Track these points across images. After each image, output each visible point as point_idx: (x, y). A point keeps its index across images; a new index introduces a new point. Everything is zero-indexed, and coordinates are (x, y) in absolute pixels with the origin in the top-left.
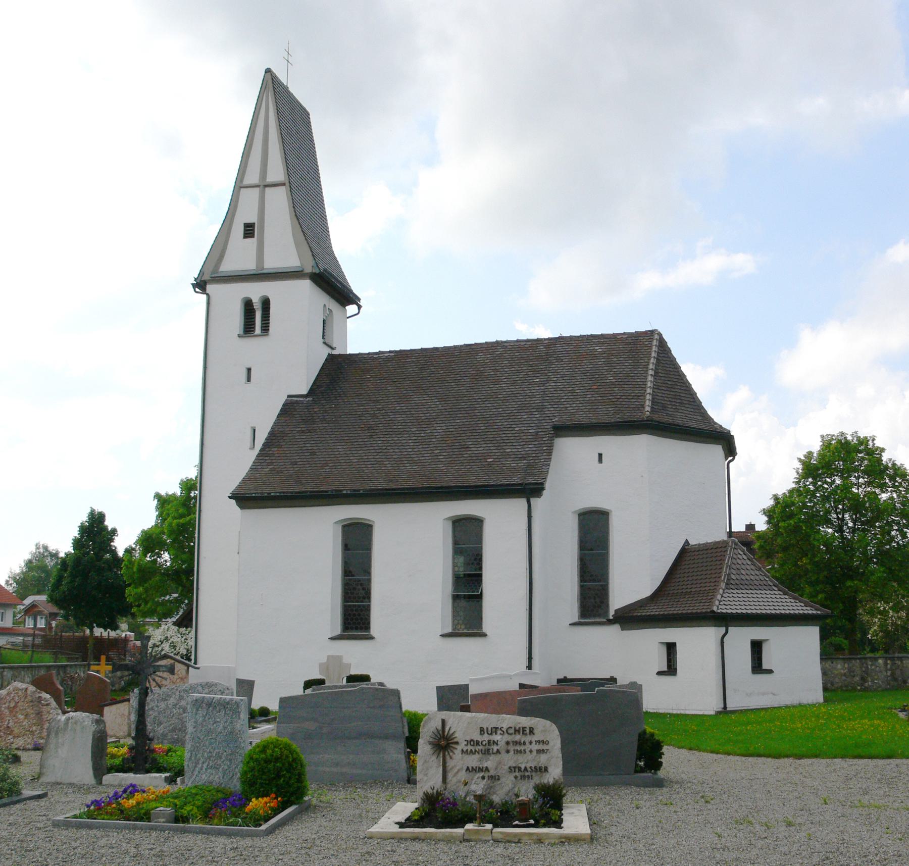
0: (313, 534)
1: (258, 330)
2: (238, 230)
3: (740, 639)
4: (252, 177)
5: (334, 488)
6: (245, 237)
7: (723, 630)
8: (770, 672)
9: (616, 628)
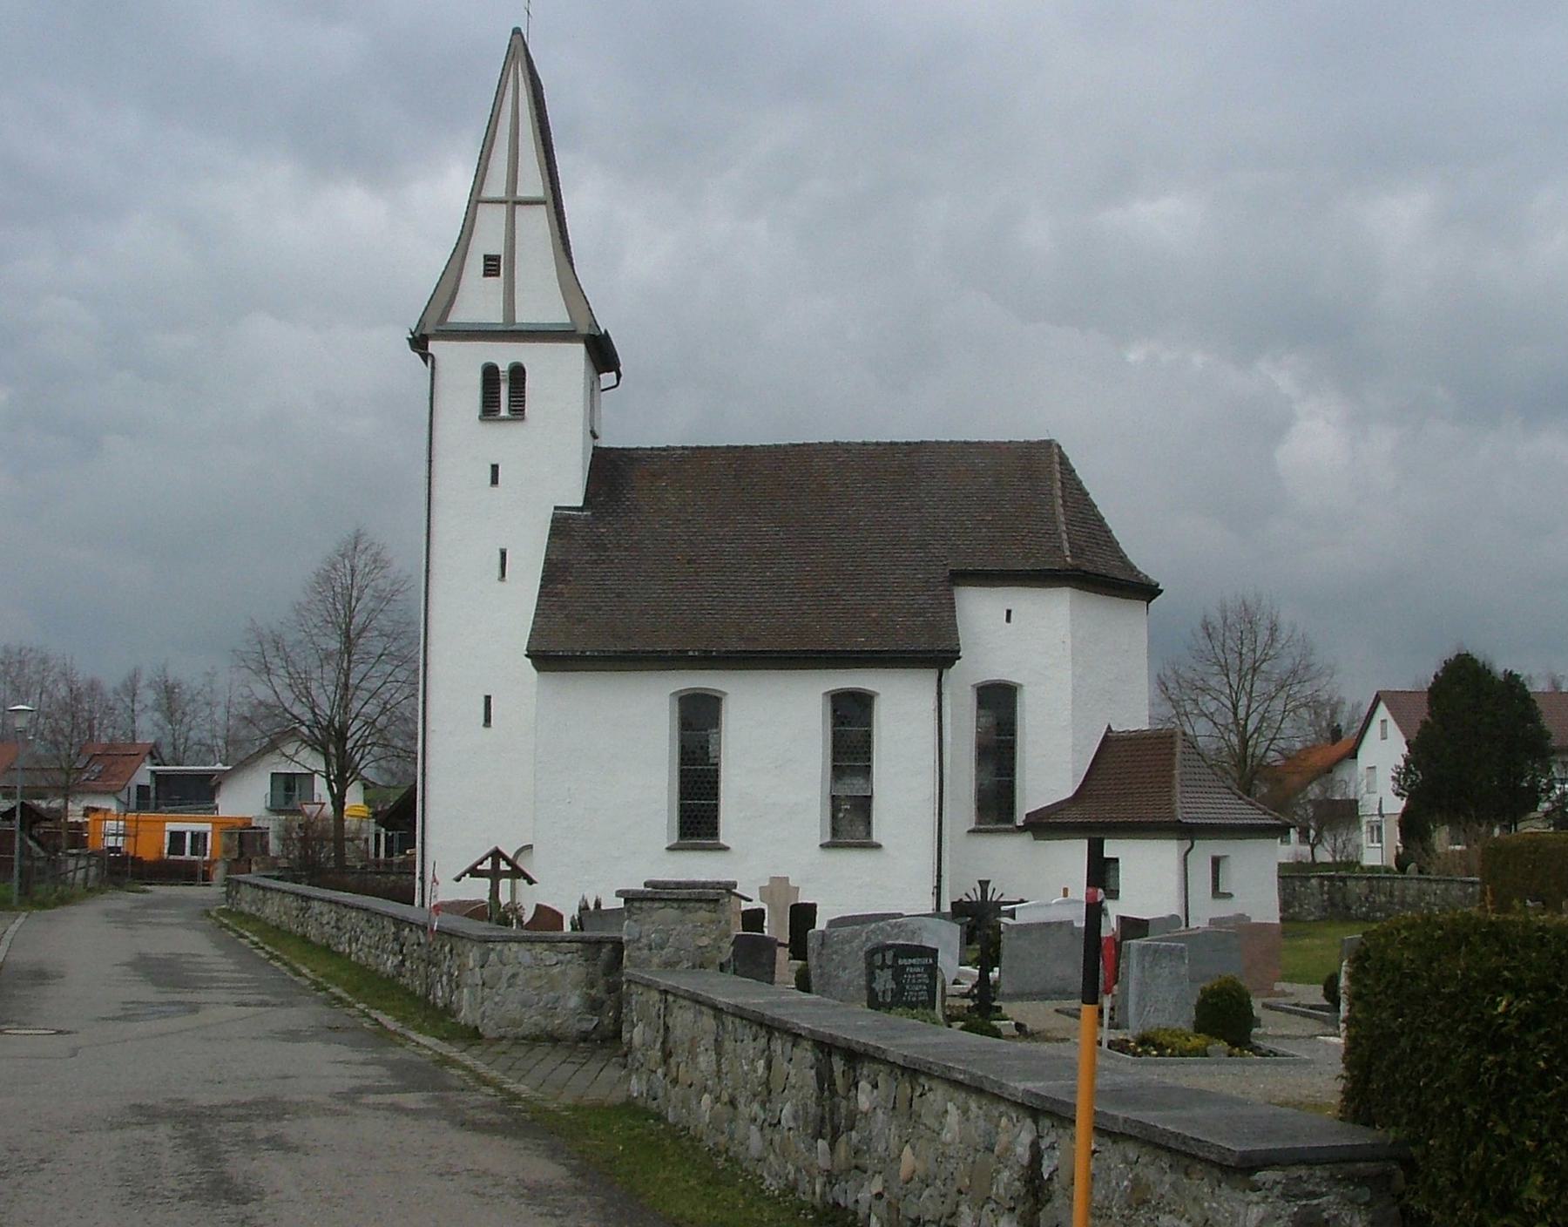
0: (643, 710)
1: (504, 412)
2: (475, 264)
3: (1206, 849)
4: (496, 187)
5: (674, 646)
6: (485, 275)
7: (1188, 843)
8: (1230, 895)
9: (1027, 838)
